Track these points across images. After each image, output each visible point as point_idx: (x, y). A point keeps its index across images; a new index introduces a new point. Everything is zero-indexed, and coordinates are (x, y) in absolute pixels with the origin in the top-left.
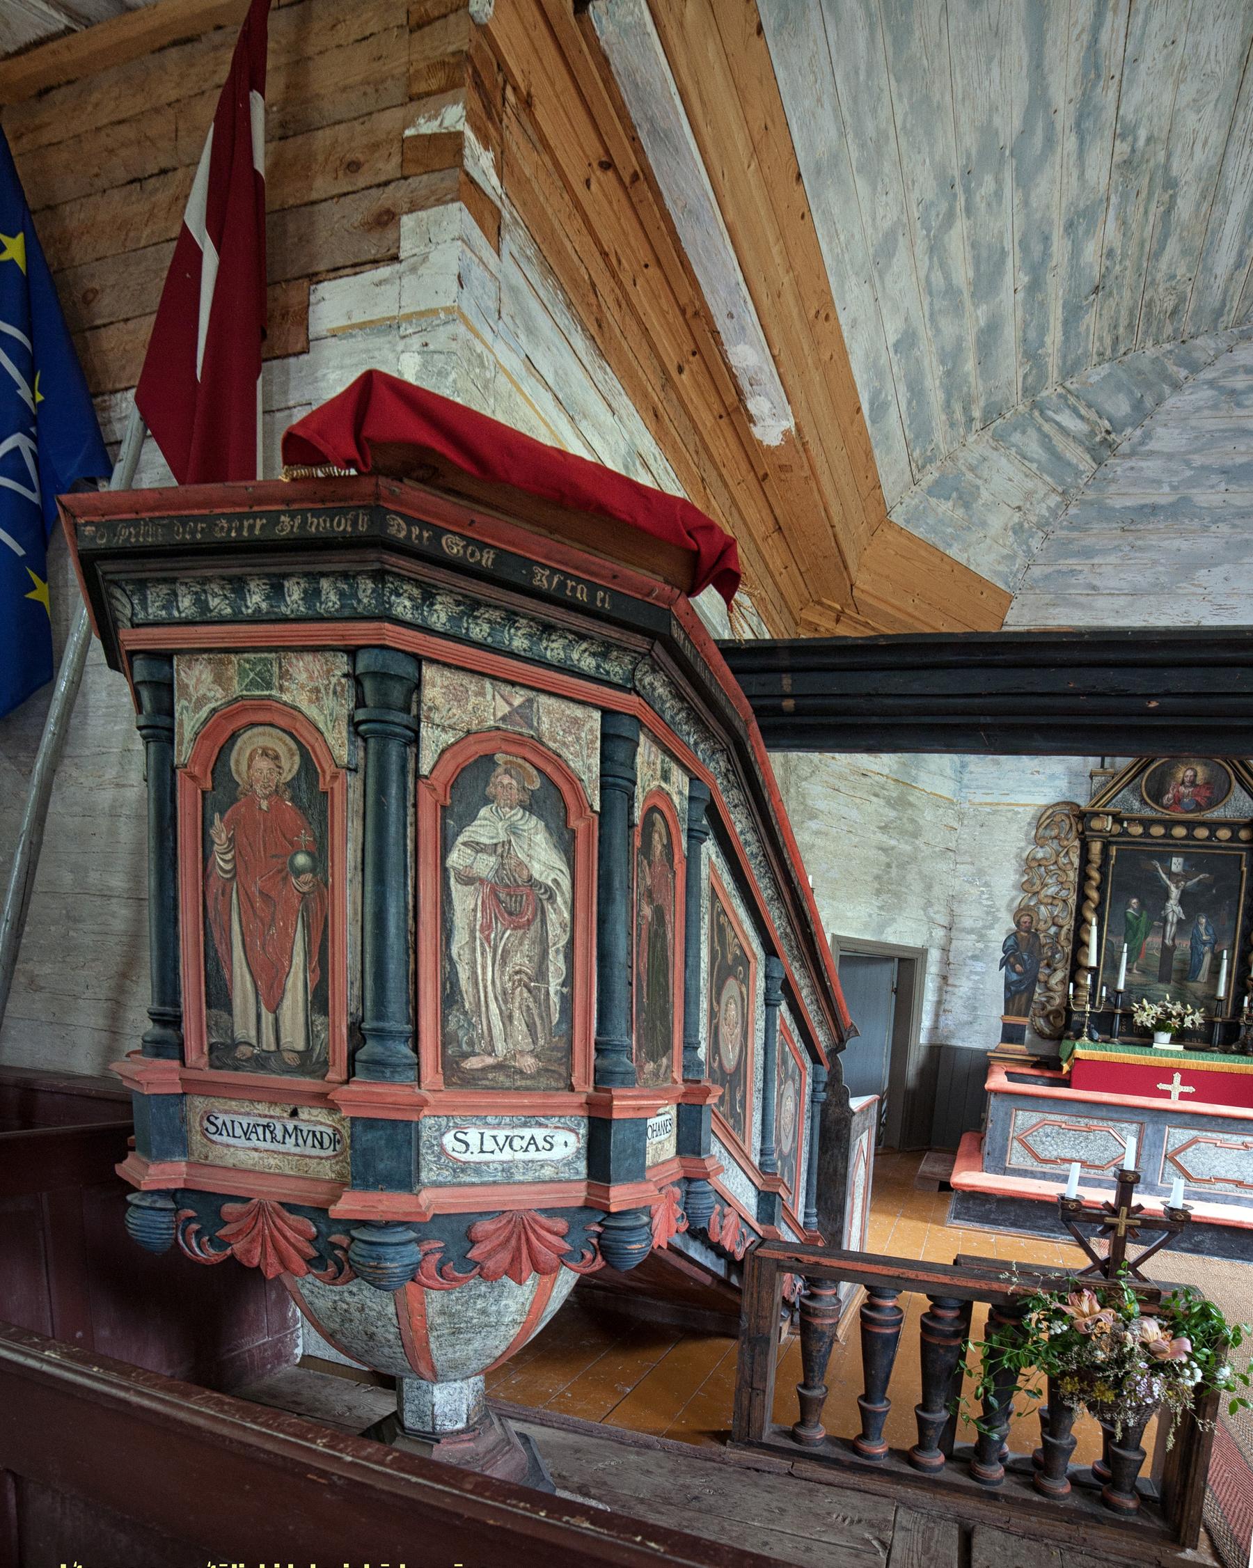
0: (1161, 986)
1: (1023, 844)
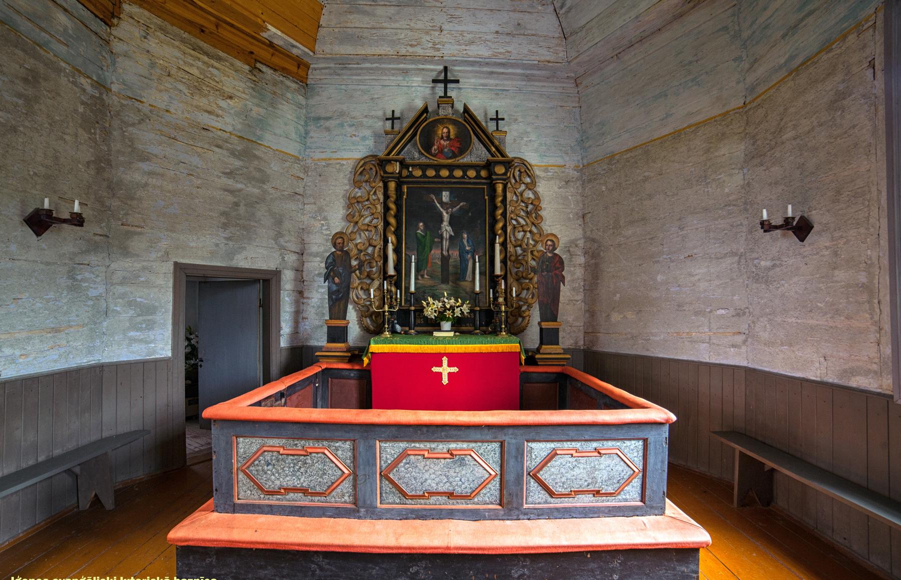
0: (444, 286)
1: (347, 187)
